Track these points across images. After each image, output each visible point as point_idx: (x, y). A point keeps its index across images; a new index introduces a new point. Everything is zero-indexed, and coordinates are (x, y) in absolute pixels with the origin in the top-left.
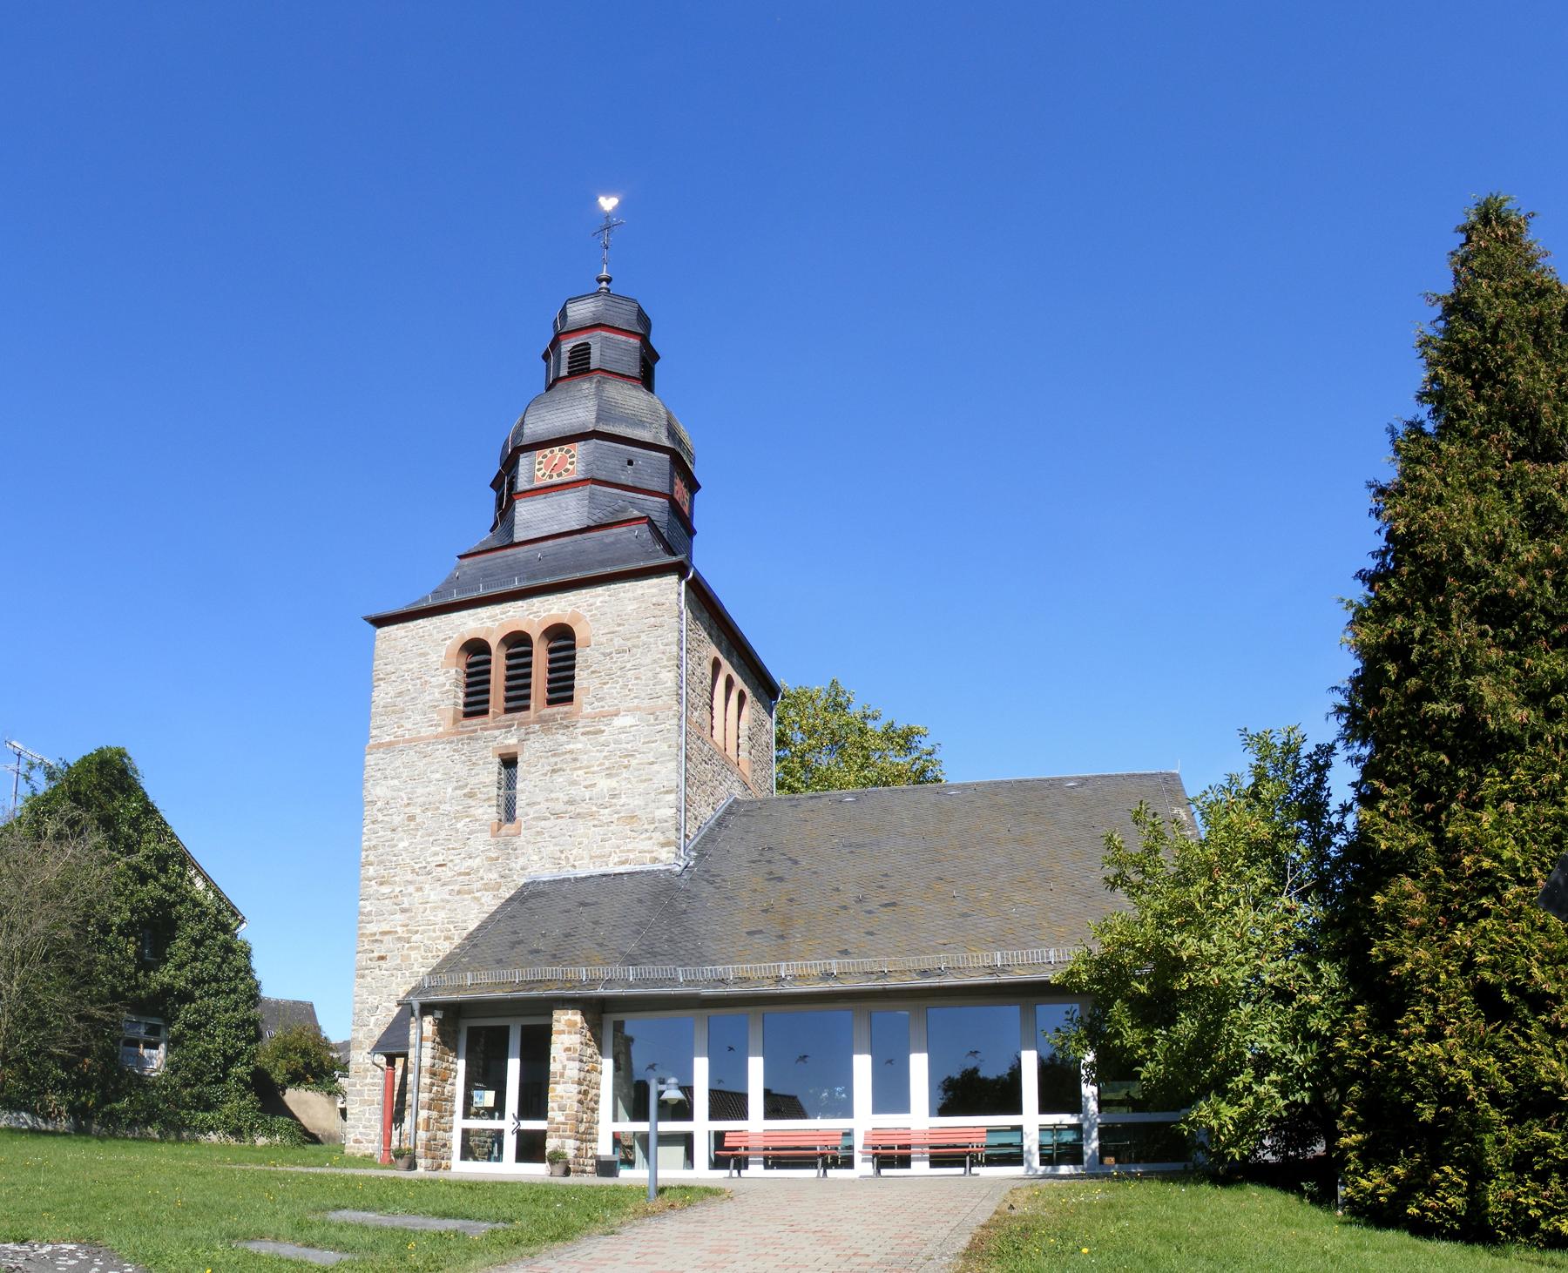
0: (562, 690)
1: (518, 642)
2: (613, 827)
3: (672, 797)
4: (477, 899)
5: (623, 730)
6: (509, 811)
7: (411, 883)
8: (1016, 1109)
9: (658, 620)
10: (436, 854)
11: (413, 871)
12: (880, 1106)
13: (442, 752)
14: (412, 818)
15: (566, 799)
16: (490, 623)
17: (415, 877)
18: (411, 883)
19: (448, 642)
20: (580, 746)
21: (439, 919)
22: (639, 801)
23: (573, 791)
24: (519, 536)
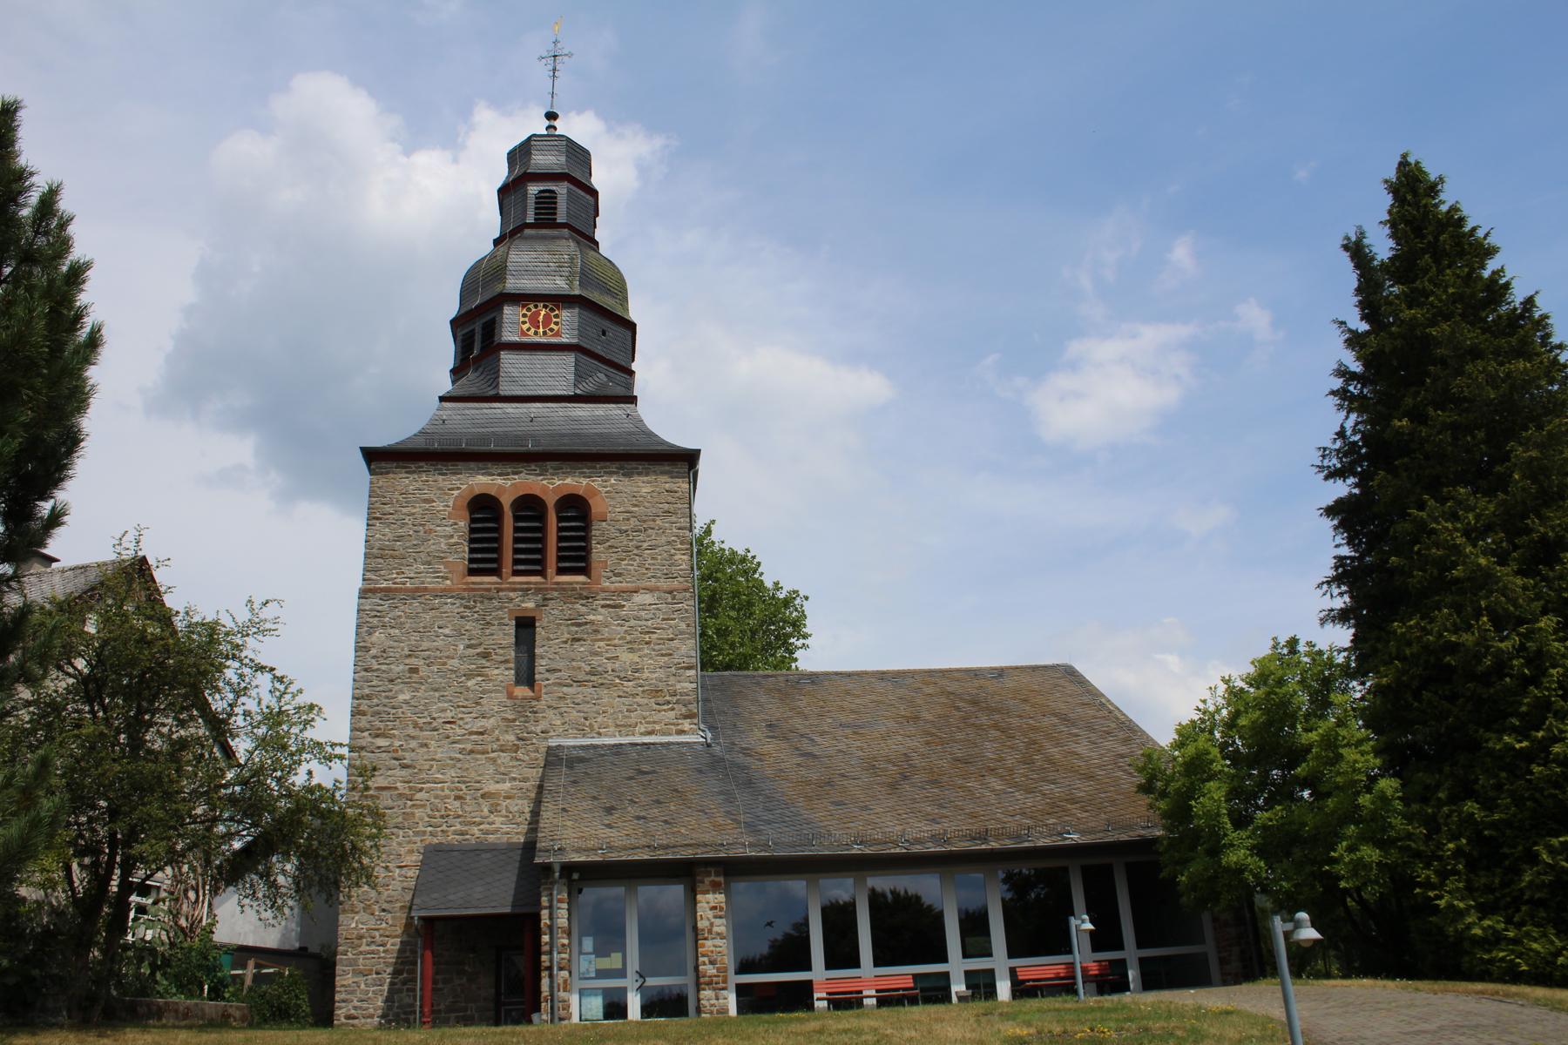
0: (577, 558)
1: (529, 506)
2: (638, 699)
3: (693, 672)
4: (494, 760)
5: (643, 607)
6: (526, 676)
7: (413, 738)
8: (807, 967)
10: (443, 710)
11: (416, 725)
13: (452, 607)
14: (414, 670)
15: (588, 669)
16: (505, 485)
18: (413, 738)
19: (456, 493)
20: (600, 618)
21: (447, 778)
22: (660, 674)
23: (595, 661)
24: (506, 389)
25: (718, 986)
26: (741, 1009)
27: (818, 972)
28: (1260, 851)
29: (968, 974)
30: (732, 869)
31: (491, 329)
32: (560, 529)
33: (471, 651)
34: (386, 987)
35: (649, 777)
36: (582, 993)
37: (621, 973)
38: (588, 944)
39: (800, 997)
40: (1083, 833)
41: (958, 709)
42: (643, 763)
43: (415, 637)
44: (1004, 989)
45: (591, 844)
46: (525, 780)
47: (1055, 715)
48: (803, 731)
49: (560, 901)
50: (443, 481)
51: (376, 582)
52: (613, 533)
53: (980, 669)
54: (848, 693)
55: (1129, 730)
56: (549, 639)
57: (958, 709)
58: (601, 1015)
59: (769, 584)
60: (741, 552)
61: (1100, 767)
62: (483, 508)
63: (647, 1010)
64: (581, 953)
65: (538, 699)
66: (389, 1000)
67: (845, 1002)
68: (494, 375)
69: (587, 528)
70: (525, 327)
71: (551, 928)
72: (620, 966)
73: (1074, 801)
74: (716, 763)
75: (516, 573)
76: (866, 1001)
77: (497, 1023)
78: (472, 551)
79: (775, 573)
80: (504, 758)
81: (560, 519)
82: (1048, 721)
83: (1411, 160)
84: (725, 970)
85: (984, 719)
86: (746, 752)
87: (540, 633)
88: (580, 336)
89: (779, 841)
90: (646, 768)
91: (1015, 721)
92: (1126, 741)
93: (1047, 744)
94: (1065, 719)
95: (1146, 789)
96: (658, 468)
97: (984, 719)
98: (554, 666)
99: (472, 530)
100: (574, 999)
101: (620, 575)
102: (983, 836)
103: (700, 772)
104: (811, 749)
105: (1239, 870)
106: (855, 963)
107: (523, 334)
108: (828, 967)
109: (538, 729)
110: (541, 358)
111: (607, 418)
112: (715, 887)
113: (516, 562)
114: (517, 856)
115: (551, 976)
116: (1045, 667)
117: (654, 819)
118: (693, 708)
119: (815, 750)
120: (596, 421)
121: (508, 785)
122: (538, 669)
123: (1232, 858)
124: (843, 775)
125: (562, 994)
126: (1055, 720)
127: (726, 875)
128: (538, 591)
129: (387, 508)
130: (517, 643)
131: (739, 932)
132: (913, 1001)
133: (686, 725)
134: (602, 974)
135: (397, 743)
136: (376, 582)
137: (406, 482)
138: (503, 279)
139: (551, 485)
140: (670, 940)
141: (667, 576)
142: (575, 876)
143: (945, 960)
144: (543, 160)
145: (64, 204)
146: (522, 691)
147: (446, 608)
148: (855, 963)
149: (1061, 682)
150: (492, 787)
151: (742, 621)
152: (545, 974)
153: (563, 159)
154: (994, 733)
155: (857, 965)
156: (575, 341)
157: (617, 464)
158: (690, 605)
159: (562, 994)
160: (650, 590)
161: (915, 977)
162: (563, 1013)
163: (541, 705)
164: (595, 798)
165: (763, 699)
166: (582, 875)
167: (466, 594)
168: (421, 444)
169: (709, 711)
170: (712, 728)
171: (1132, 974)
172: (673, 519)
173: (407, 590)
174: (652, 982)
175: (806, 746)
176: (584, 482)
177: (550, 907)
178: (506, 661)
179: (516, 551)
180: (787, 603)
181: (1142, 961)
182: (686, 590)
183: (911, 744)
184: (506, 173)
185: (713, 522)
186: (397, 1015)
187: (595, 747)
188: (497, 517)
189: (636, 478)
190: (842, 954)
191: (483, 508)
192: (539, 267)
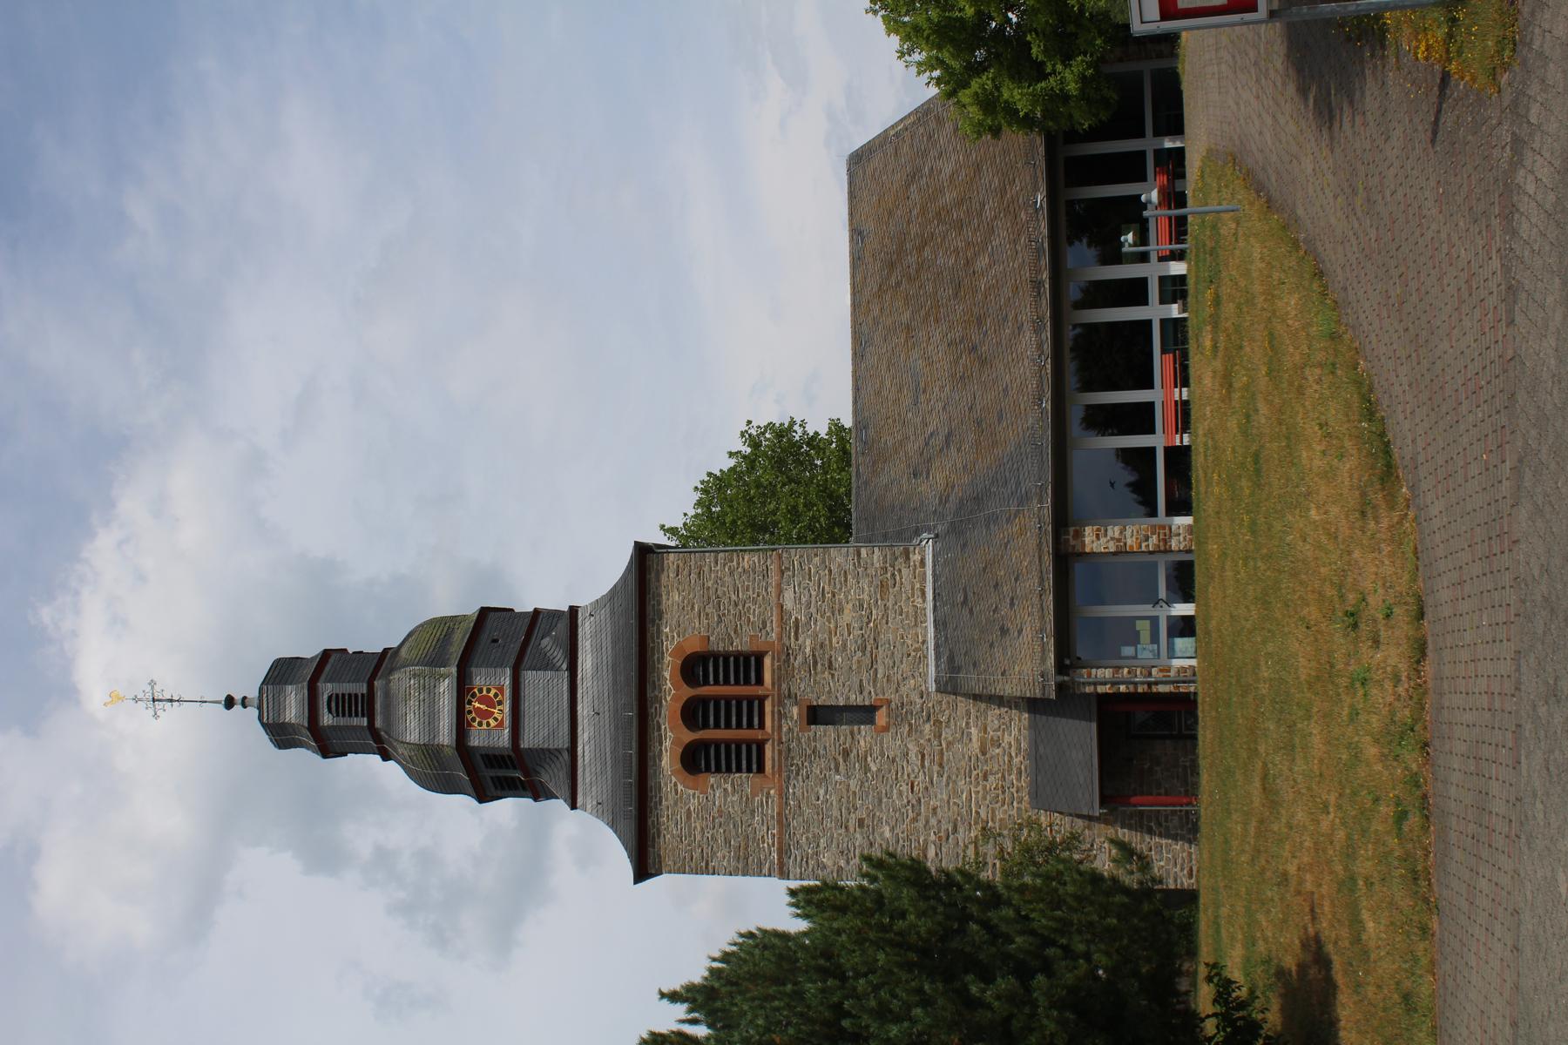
0: (747, 665)
1: (692, 714)
2: (890, 604)
3: (864, 552)
4: (949, 744)
5: (797, 600)
6: (865, 714)
7: (927, 822)
9: (695, 571)
10: (900, 793)
11: (915, 820)
12: (1143, 300)
13: (797, 788)
14: (861, 822)
15: (859, 654)
16: (670, 739)
17: (922, 819)
18: (927, 822)
19: (680, 787)
20: (808, 642)
22: (865, 583)
23: (851, 646)
24: (563, 741)
25: (1167, 534)
27: (1157, 441)
28: (1067, 59)
29: (1162, 302)
30: (1063, 520)
31: (494, 759)
32: (716, 682)
33: (842, 768)
34: (1164, 841)
35: (970, 595)
36: (1172, 655)
37: (1154, 621)
38: (1128, 651)
39: (1179, 459)
40: (1036, 189)
41: (898, 284)
42: (955, 600)
43: (828, 823)
44: (1177, 268)
45: (1038, 649)
46: (968, 714)
47: (908, 186)
49: (1089, 675)
51: (772, 863)
53: (852, 254)
55: (923, 113)
56: (830, 692)
57: (898, 284)
58: (1191, 640)
59: (732, 462)
60: (697, 496)
61: (968, 156)
62: (694, 760)
63: (1188, 598)
64: (1135, 657)
66: (1175, 838)
68: (545, 755)
69: (716, 656)
70: (493, 723)
71: (1113, 684)
72: (1148, 622)
73: (1003, 191)
74: (956, 530)
75: (762, 726)
76: (1185, 397)
77: (1194, 738)
78: (739, 770)
79: (719, 452)
80: (947, 734)
81: (706, 683)
82: (915, 195)
84: (1153, 527)
85: (912, 259)
86: (944, 500)
87: (823, 700)
88: (502, 665)
89: (1037, 475)
90: (960, 598)
92: (939, 121)
94: (913, 177)
95: (996, 132)
96: (653, 585)
97: (912, 259)
98: (857, 687)
99: (718, 770)
100: (1176, 663)
101: (764, 624)
102: (1037, 285)
103: (965, 545)
104: (941, 437)
105: (1083, 79)
106: (1150, 406)
107: (501, 724)
108: (1152, 431)
109: (919, 701)
110: (527, 706)
111: (595, 635)
112: (1079, 535)
113: (750, 725)
114: (1042, 719)
115: (1156, 683)
116: (850, 183)
117: (1014, 590)
118: (898, 551)
119: (943, 432)
120: (597, 649)
121: (973, 730)
122: (859, 702)
123: (1072, 87)
124: (971, 409)
125: (1172, 674)
126: (913, 188)
127: (1066, 525)
128: (781, 703)
129: (696, 855)
130: (833, 723)
131: (1120, 514)
132: (1185, 355)
133: (916, 557)
134: (1155, 638)
135: (933, 837)
136: (772, 863)
138: (440, 747)
139: (671, 691)
140: (1130, 577)
141: (765, 575)
142: (1067, 662)
143: (1148, 323)
144: (293, 708)
145: (717, 954)
146: (881, 717)
147: (799, 793)
148: (1150, 406)
149: (869, 171)
150: (975, 745)
151: (782, 493)
152: (1154, 689)
154: (927, 252)
155: (1152, 405)
156: (508, 671)
157: (649, 625)
158: (795, 554)
159: (1172, 674)
160: (780, 592)
161: (1163, 352)
162: (1189, 673)
163: (895, 698)
164: (992, 645)
165: (884, 479)
166: (1066, 660)
167: (784, 774)
168: (630, 826)
170: (917, 532)
171: (1168, 144)
172: (706, 569)
173: (780, 832)
174: (1162, 594)
175: (938, 441)
176: (668, 659)
177: (1095, 684)
178: (852, 733)
179: (739, 726)
180: (754, 443)
181: (1158, 133)
182: (780, 557)
183: (938, 336)
184: (309, 753)
185: (662, 527)
186: (1189, 831)
187: (937, 646)
188: (704, 745)
189: (663, 607)
190: (1141, 418)
191: (694, 760)
192: (422, 711)
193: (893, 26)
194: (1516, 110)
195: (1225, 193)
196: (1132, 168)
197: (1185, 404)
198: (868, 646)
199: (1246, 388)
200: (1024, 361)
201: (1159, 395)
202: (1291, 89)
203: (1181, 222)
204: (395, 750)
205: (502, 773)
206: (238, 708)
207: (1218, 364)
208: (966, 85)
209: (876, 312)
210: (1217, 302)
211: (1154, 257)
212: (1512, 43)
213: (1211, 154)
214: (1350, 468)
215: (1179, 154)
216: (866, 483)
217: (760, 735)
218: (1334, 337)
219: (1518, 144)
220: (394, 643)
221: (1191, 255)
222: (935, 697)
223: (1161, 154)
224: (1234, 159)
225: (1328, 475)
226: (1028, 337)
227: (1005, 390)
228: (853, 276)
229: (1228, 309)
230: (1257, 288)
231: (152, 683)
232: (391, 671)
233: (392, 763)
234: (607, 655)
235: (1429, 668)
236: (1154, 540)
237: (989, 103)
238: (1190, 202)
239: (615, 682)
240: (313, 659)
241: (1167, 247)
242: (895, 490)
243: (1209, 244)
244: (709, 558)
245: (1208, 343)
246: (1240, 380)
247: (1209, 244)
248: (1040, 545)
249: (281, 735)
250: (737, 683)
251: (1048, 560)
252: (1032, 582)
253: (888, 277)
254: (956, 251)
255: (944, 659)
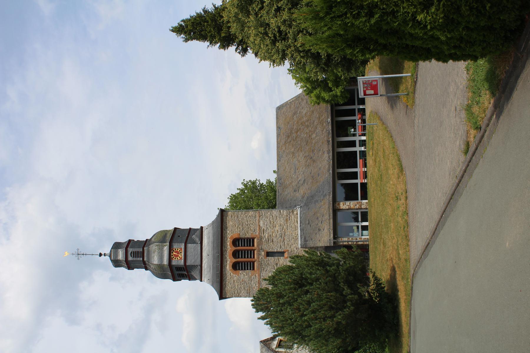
0: (250, 241)
1: (235, 254)
12: (355, 146)
22: (282, 219)
23: (278, 236)
24: (198, 263)
26: (366, 199)
27: (358, 181)
28: (337, 87)
29: (360, 146)
30: (334, 200)
31: (179, 268)
32: (242, 246)
36: (362, 235)
37: (358, 227)
38: (351, 234)
39: (364, 186)
40: (328, 118)
41: (290, 141)
42: (306, 223)
44: (363, 138)
48: (297, 182)
50: (228, 278)
52: (243, 232)
53: (277, 133)
54: (284, 170)
55: (298, 97)
57: (290, 141)
59: (238, 191)
62: (235, 267)
65: (288, 251)
67: (365, 175)
68: (193, 267)
71: (348, 242)
73: (319, 118)
74: (306, 205)
75: (254, 257)
78: (248, 269)
81: (239, 246)
83: (171, 29)
85: (294, 135)
89: (328, 189)
90: (307, 222)
91: (295, 127)
93: (303, 120)
94: (295, 114)
95: (319, 104)
99: (242, 269)
100: (363, 237)
102: (328, 142)
104: (302, 181)
105: (341, 92)
108: (357, 179)
110: (188, 253)
112: (339, 204)
116: (277, 115)
118: (291, 211)
120: (208, 238)
123: (339, 94)
126: (295, 116)
128: (259, 251)
132: (365, 160)
133: (295, 213)
137: (229, 287)
139: (229, 248)
141: (255, 217)
143: (356, 151)
144: (121, 255)
149: (282, 112)
151: (255, 197)
153: (119, 250)
155: (357, 172)
156: (183, 244)
158: (263, 212)
160: (259, 222)
161: (360, 159)
163: (290, 249)
165: (286, 193)
169: (291, 207)
170: (295, 206)
171: (361, 107)
174: (360, 220)
175: (302, 182)
176: (229, 239)
180: (245, 185)
181: (358, 104)
187: (301, 236)
190: (354, 176)
191: (235, 267)
192: (158, 256)
193: (294, 77)
194: (414, 111)
195: (375, 121)
196: (352, 113)
197: (366, 172)
198: (283, 236)
199: (379, 161)
200: (325, 161)
201: (359, 170)
202: (387, 102)
203: (365, 127)
204: (150, 266)
205: (180, 272)
206: (103, 256)
207: (373, 158)
208: (312, 92)
209: (284, 149)
210: (373, 144)
211: (357, 135)
212: (414, 102)
213: (371, 112)
214: (396, 171)
215: (364, 109)
216: (281, 194)
217: (253, 260)
218: (394, 148)
219: (415, 116)
220: (149, 238)
221: (367, 134)
222: (300, 249)
223: (360, 110)
224: (376, 113)
225: (393, 174)
226: (326, 155)
227: (320, 168)
228: (277, 139)
229: (375, 145)
230: (381, 140)
231: (78, 249)
232: (150, 245)
233: (148, 271)
234: (211, 239)
235: (408, 200)
236: (358, 206)
237: (318, 97)
238: (367, 122)
239: (213, 246)
240: (125, 242)
241: (361, 132)
242: (289, 195)
243: (371, 131)
244: (240, 213)
245: (371, 153)
246: (378, 159)
247: (371, 131)
248: (329, 207)
249: (117, 263)
250: (247, 246)
251: (331, 211)
252: (327, 217)
253: (288, 139)
254: (307, 133)
255: (303, 239)
